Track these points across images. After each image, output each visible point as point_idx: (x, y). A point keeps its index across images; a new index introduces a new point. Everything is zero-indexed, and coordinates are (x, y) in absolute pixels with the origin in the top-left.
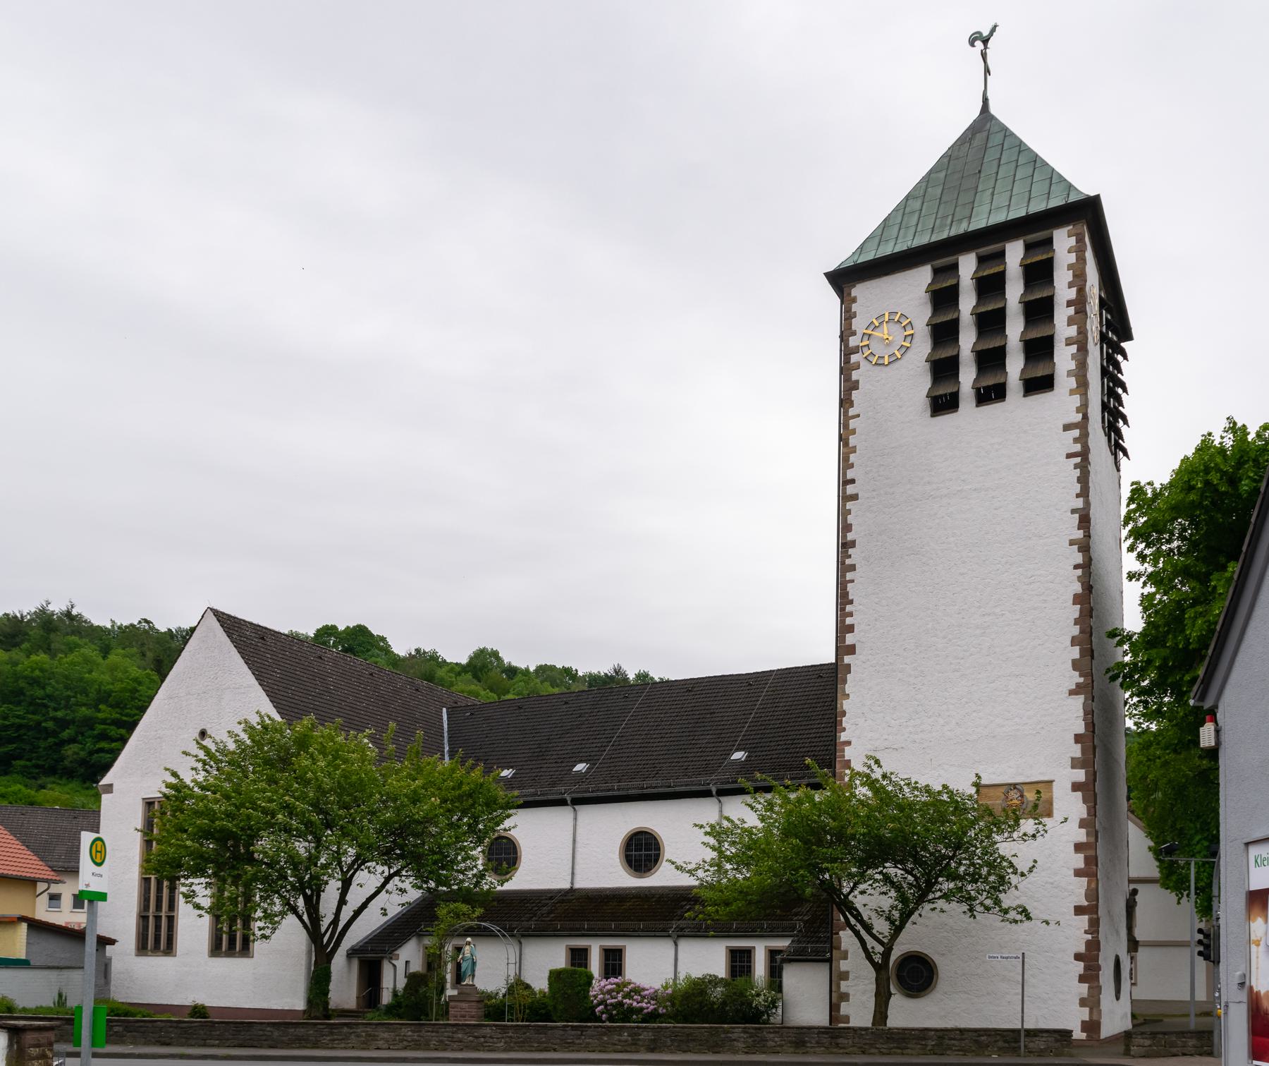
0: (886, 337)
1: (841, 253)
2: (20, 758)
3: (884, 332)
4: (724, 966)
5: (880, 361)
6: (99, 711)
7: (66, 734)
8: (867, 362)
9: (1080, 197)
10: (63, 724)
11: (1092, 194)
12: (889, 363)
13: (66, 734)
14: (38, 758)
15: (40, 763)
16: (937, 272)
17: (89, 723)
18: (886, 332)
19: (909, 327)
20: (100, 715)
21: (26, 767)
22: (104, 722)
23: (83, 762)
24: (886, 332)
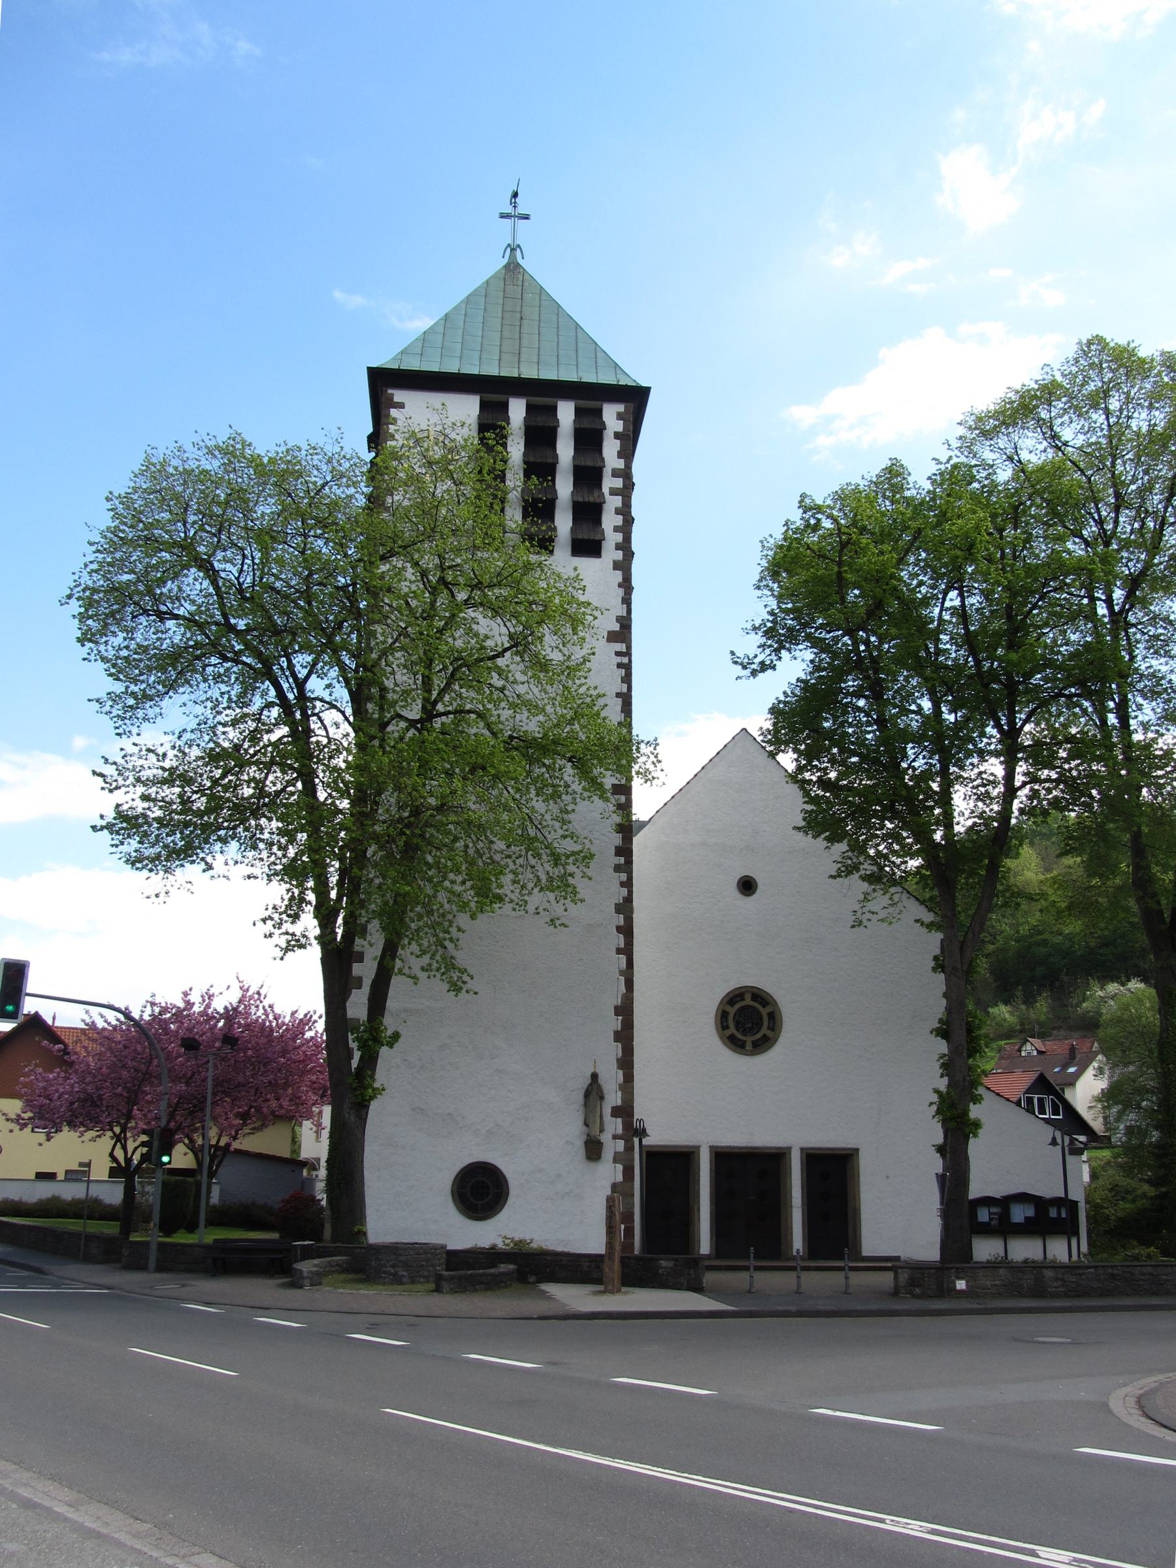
1: (384, 358)
11: (644, 383)
16: (484, 406)
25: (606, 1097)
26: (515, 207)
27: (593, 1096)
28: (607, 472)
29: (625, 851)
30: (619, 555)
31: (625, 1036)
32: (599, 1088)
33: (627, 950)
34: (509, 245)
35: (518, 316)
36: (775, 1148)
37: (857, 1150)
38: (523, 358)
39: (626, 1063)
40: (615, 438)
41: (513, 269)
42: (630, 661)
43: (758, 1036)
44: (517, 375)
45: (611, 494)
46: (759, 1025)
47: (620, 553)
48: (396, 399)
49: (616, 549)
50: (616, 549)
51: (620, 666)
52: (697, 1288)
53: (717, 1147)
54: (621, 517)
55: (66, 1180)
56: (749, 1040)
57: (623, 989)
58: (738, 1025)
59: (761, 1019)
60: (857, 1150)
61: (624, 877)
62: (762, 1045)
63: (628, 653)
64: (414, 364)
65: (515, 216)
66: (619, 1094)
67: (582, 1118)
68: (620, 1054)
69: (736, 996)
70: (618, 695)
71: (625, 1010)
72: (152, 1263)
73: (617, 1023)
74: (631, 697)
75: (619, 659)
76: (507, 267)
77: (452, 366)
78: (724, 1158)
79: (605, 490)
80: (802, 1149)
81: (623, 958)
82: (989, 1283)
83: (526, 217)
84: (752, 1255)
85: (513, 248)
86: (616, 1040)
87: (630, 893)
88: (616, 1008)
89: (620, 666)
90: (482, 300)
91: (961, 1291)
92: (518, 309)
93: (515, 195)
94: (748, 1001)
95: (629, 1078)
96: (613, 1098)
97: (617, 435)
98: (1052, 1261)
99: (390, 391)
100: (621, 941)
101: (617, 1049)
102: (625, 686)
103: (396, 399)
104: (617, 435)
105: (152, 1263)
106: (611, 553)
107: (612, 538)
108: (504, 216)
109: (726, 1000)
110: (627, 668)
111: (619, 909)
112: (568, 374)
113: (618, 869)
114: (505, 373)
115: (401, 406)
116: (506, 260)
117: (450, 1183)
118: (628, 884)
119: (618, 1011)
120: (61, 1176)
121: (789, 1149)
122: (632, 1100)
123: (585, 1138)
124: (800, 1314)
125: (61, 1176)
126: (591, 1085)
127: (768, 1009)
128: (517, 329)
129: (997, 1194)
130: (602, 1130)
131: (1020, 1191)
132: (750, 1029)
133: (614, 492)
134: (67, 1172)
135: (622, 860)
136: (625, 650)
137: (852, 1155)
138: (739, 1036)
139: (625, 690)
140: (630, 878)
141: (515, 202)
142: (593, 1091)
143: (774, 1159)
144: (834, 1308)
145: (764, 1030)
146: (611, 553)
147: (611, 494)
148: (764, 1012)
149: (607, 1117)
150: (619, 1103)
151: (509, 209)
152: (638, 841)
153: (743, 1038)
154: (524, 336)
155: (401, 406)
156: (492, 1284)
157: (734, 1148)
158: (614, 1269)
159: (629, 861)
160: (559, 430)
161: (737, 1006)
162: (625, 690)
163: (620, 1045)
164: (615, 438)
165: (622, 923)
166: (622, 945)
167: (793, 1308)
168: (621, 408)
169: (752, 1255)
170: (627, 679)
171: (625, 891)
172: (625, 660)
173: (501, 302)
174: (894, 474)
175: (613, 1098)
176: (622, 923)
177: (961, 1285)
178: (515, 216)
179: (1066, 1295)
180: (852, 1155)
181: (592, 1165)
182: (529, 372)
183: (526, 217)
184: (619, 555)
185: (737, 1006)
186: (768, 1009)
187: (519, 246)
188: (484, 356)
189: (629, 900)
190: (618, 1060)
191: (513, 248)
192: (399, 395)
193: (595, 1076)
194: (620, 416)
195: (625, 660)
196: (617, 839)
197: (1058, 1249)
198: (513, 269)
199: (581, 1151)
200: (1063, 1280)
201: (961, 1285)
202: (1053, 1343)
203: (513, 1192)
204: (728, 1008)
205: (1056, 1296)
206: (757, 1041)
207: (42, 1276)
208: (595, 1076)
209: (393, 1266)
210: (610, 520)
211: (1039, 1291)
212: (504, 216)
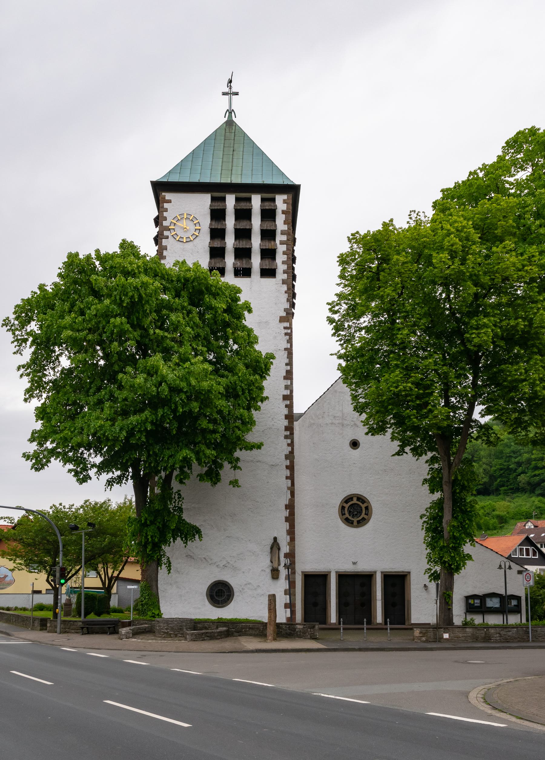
0: (185, 227)
1: (157, 177)
2: (503, 486)
3: (184, 223)
4: (412, 586)
5: (181, 240)
6: (533, 454)
7: (520, 470)
8: (173, 239)
9: (292, 184)
10: (519, 464)
11: (297, 183)
12: (186, 242)
13: (520, 470)
14: (511, 484)
15: (511, 487)
16: (213, 199)
17: (529, 461)
18: (185, 224)
19: (197, 225)
20: (533, 457)
21: (505, 490)
22: (535, 460)
23: (529, 483)
24: (185, 224)
25: (281, 548)
26: (230, 88)
27: (275, 548)
28: (278, 232)
29: (290, 429)
30: (285, 276)
31: (291, 519)
32: (278, 545)
33: (291, 477)
34: (228, 110)
35: (232, 149)
36: (368, 572)
37: (409, 573)
38: (233, 172)
39: (291, 532)
40: (282, 213)
41: (230, 124)
42: (292, 331)
43: (360, 518)
44: (229, 182)
45: (280, 244)
46: (361, 513)
47: (286, 275)
48: (167, 198)
49: (284, 273)
50: (284, 273)
51: (286, 334)
52: (314, 638)
53: (339, 572)
54: (286, 256)
55: (46, 593)
56: (355, 520)
57: (289, 496)
58: (350, 512)
59: (362, 510)
60: (409, 573)
61: (289, 441)
62: (362, 522)
63: (290, 328)
64: (175, 178)
65: (230, 94)
66: (288, 547)
67: (269, 559)
68: (288, 528)
69: (349, 499)
70: (285, 349)
71: (291, 507)
72: (58, 630)
73: (287, 513)
74: (292, 350)
75: (286, 331)
76: (226, 122)
77: (196, 178)
78: (342, 577)
79: (278, 242)
80: (382, 572)
81: (289, 482)
82: (461, 635)
83: (237, 94)
84: (365, 623)
85: (230, 112)
86: (286, 521)
87: (293, 449)
88: (286, 506)
89: (286, 334)
90: (213, 141)
91: (446, 639)
92: (232, 146)
93: (230, 82)
94: (355, 501)
95: (293, 539)
96: (285, 549)
97: (283, 212)
98: (510, 625)
99: (163, 194)
100: (288, 473)
101: (287, 526)
102: (289, 345)
103: (167, 198)
104: (283, 212)
105: (58, 630)
106: (281, 276)
107: (281, 267)
108: (224, 94)
109: (344, 500)
110: (289, 336)
111: (287, 457)
112: (257, 180)
113: (286, 437)
114: (223, 181)
115: (169, 201)
116: (226, 119)
117: (206, 590)
118: (291, 445)
119: (287, 507)
120: (44, 592)
121: (375, 572)
122: (294, 550)
123: (271, 568)
124: (360, 650)
125: (44, 592)
126: (273, 543)
127: (365, 505)
128: (231, 157)
129: (481, 594)
130: (279, 565)
131: (492, 592)
132: (356, 515)
133: (282, 243)
134: (47, 590)
135: (288, 433)
136: (288, 326)
137: (406, 575)
138: (350, 518)
139: (289, 347)
140: (292, 442)
141: (230, 86)
142: (275, 545)
143: (323, 577)
144: (378, 647)
145: (363, 515)
146: (281, 276)
147: (280, 244)
148: (363, 506)
149: (282, 558)
150: (288, 551)
151: (227, 90)
152: (296, 425)
153: (353, 519)
154: (235, 160)
155: (169, 201)
156: (212, 637)
157: (348, 572)
158: (270, 630)
159: (292, 434)
160: (252, 210)
161: (350, 504)
162: (289, 347)
163: (288, 524)
164: (282, 213)
165: (288, 464)
166: (289, 475)
167: (357, 647)
168: (285, 197)
169: (365, 623)
170: (290, 341)
171: (290, 449)
172: (289, 331)
173: (223, 142)
174: (42, 287)
175: (285, 549)
176: (288, 464)
177: (446, 636)
178: (230, 94)
179: (501, 642)
180: (406, 575)
181: (275, 581)
182: (237, 180)
183: (237, 94)
184: (285, 276)
185: (350, 504)
186: (365, 505)
187: (233, 110)
188: (213, 172)
189: (292, 452)
190: (287, 531)
191: (230, 112)
192: (168, 196)
193: (275, 539)
194: (285, 202)
195: (289, 331)
196: (286, 423)
197: (513, 619)
198: (230, 124)
199: (269, 575)
200: (499, 634)
201: (446, 636)
202: (476, 663)
203: (236, 594)
204: (345, 505)
205: (496, 642)
206: (359, 520)
207: (8, 637)
208: (275, 539)
209: (167, 629)
210: (280, 258)
211: (487, 639)
212: (224, 94)
